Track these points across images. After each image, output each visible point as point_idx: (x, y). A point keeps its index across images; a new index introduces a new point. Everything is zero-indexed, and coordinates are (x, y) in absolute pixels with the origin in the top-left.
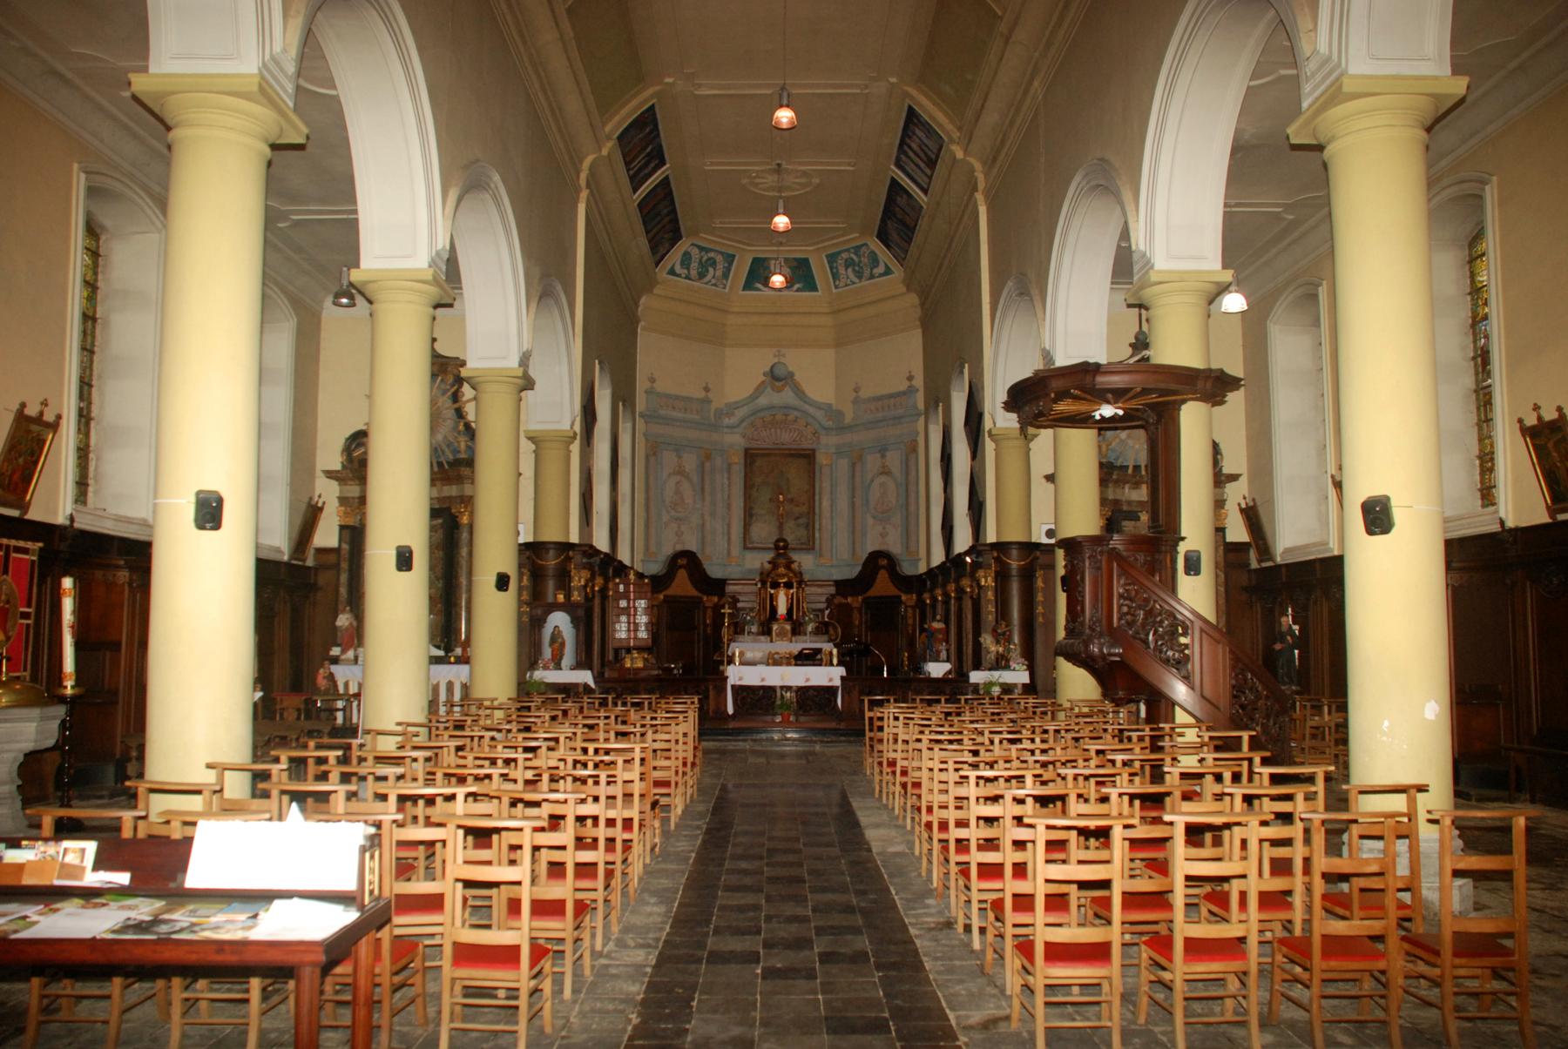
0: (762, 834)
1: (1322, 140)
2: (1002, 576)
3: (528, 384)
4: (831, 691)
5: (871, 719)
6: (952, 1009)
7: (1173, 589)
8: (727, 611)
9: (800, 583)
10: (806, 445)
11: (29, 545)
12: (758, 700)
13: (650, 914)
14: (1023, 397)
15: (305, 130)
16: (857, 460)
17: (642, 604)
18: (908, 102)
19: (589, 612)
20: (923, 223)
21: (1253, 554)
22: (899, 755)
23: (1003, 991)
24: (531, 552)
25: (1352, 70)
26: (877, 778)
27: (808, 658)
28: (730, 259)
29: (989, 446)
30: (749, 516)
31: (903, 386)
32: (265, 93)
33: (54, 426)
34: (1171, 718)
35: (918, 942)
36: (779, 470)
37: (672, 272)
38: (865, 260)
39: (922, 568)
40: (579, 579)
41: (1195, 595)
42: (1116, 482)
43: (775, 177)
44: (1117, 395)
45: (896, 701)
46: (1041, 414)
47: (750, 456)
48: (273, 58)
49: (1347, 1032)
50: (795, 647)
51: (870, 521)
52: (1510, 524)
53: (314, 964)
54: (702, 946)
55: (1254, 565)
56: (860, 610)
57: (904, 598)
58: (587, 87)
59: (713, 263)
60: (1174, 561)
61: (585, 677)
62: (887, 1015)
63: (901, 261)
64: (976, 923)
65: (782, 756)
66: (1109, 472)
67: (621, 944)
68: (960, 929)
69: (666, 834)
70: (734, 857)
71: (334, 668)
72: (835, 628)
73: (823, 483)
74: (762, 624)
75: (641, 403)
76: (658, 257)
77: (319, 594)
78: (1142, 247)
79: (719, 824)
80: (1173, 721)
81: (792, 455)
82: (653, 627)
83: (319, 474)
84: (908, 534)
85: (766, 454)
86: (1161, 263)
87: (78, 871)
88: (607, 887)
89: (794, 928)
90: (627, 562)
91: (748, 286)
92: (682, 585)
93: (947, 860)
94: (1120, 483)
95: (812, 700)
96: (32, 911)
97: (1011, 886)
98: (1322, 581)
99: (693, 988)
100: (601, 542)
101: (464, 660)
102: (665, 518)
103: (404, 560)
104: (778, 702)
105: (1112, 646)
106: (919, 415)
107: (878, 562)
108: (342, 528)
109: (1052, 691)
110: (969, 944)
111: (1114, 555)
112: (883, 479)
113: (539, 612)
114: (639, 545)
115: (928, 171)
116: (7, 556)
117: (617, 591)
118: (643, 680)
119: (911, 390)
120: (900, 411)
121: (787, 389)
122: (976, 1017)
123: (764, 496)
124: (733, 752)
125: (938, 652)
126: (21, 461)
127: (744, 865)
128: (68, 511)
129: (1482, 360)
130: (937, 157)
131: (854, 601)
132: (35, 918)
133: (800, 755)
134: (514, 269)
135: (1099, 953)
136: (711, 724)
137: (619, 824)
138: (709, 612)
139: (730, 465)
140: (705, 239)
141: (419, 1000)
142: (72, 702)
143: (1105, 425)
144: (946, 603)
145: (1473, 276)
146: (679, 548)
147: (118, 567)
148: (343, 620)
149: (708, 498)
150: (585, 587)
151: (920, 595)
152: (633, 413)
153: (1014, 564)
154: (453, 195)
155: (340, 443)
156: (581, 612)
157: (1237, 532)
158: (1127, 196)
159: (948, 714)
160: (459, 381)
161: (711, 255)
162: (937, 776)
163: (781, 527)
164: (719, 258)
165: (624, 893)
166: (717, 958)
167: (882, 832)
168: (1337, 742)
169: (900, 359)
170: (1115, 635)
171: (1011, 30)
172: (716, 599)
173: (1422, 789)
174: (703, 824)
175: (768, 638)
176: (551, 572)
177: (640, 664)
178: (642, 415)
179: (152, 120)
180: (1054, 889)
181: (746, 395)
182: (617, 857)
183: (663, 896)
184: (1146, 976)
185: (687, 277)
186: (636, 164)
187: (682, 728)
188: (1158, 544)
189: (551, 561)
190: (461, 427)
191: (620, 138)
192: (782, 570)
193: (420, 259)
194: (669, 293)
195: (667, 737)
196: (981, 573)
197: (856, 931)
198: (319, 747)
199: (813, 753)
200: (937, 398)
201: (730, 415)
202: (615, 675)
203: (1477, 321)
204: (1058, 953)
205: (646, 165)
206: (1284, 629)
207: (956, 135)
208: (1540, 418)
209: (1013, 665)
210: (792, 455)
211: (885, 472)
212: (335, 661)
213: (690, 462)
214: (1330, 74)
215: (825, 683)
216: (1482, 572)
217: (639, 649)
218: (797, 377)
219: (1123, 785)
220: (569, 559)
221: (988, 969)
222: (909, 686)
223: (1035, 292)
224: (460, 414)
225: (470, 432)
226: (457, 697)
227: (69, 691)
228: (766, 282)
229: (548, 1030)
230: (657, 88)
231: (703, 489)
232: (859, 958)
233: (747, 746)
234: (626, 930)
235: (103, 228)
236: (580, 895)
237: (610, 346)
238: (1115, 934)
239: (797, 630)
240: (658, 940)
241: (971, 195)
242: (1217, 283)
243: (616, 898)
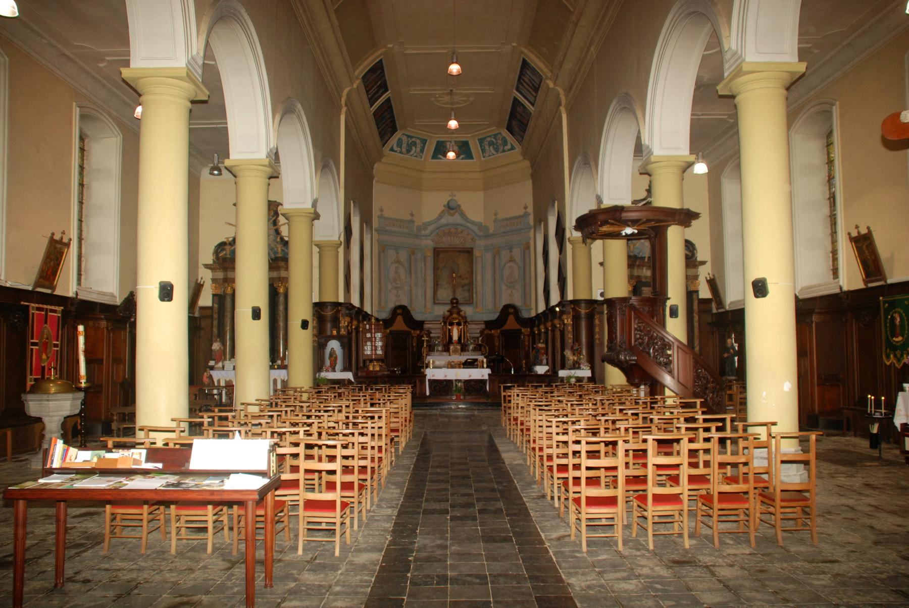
0: (447, 456)
1: (734, 94)
2: (576, 318)
3: (316, 216)
4: (483, 382)
5: (505, 396)
7: (663, 324)
8: (425, 338)
9: (465, 322)
10: (468, 246)
11: (57, 308)
12: (443, 387)
14: (583, 223)
15: (208, 93)
16: (496, 253)
17: (379, 335)
18: (523, 56)
19: (350, 340)
20: (532, 123)
21: (714, 305)
22: (519, 415)
23: (568, 524)
24: (319, 307)
25: (748, 59)
26: (508, 427)
27: (470, 364)
28: (424, 142)
29: (569, 247)
30: (436, 285)
31: (522, 212)
32: (190, 77)
33: (68, 245)
34: (662, 393)
35: (527, 504)
36: (453, 260)
37: (392, 150)
39: (533, 314)
40: (344, 323)
41: (675, 329)
42: (639, 266)
43: (449, 97)
44: (633, 223)
45: (518, 386)
46: (593, 233)
47: (437, 252)
48: (192, 57)
49: (732, 539)
50: (463, 358)
51: (504, 288)
52: (845, 289)
53: (253, 500)
54: (420, 507)
55: (714, 311)
56: (499, 337)
57: (523, 330)
58: (345, 52)
59: (415, 144)
60: (664, 311)
61: (349, 376)
63: (520, 142)
64: (556, 495)
65: (457, 417)
66: (633, 261)
67: (379, 506)
68: (549, 498)
69: (397, 456)
70: (433, 467)
71: (212, 372)
73: (478, 268)
77: (202, 332)
78: (647, 143)
79: (423, 453)
80: (664, 394)
82: (385, 348)
83: (200, 265)
84: (525, 294)
85: (446, 251)
86: (657, 151)
87: (136, 462)
88: (372, 478)
89: (465, 498)
90: (369, 312)
91: (435, 157)
92: (400, 325)
93: (542, 465)
94: (640, 266)
95: (472, 386)
96: (123, 480)
97: (572, 474)
98: (735, 321)
99: (417, 524)
100: (356, 302)
101: (284, 367)
102: (390, 287)
103: (256, 314)
105: (631, 355)
107: (509, 310)
108: (214, 295)
109: (603, 381)
110: (553, 505)
111: (632, 307)
112: (511, 264)
113: (323, 340)
114: (375, 302)
116: (46, 314)
117: (364, 328)
118: (380, 377)
119: (526, 215)
122: (555, 535)
124: (431, 415)
125: (542, 361)
126: (52, 263)
127: (439, 470)
128: (75, 290)
129: (832, 199)
132: (125, 482)
133: (466, 417)
134: (309, 155)
135: (611, 501)
136: (418, 401)
137: (376, 448)
138: (415, 339)
139: (425, 258)
140: (410, 131)
141: (286, 529)
142: (86, 390)
143: (629, 238)
144: (546, 332)
145: (828, 153)
146: (398, 304)
147: (101, 319)
148: (216, 346)
149: (413, 277)
150: (347, 326)
152: (371, 229)
153: (583, 311)
154: (204, 28)
155: (211, 249)
156: (346, 340)
157: (705, 293)
158: (639, 115)
159: (546, 393)
161: (414, 140)
162: (545, 430)
163: (454, 292)
164: (418, 142)
165: (379, 484)
166: (426, 512)
167: (511, 454)
168: (741, 404)
169: (520, 197)
170: (632, 350)
171: (578, 20)
172: (418, 332)
173: (774, 424)
174: (416, 451)
175: (454, 354)
176: (329, 319)
177: (378, 369)
178: (376, 230)
179: (131, 90)
180: (591, 474)
182: (376, 465)
183: (398, 485)
184: (636, 514)
185: (401, 152)
186: (372, 91)
187: (403, 402)
189: (329, 313)
190: (278, 240)
191: (363, 78)
192: (455, 316)
193: (262, 154)
194: (390, 161)
195: (396, 406)
196: (564, 317)
197: (496, 500)
198: (220, 411)
199: (474, 416)
200: (541, 219)
201: (425, 229)
202: (364, 374)
203: (830, 179)
204: (593, 501)
205: (377, 92)
206: (729, 345)
207: (549, 74)
208: (859, 233)
209: (582, 366)
211: (512, 260)
212: (212, 368)
213: (403, 256)
214: (737, 60)
215: (480, 378)
216: (817, 317)
217: (377, 360)
220: (338, 311)
221: (562, 515)
222: (526, 378)
223: (592, 163)
224: (277, 232)
225: (286, 244)
226: (279, 387)
227: (83, 385)
228: (445, 155)
229: (348, 542)
230: (383, 50)
232: (498, 511)
233: (437, 412)
234: (380, 500)
235: (86, 135)
236: (345, 500)
237: (359, 193)
238: (620, 492)
239: (464, 349)
241: (558, 109)
242: (792, 73)
243: (375, 484)
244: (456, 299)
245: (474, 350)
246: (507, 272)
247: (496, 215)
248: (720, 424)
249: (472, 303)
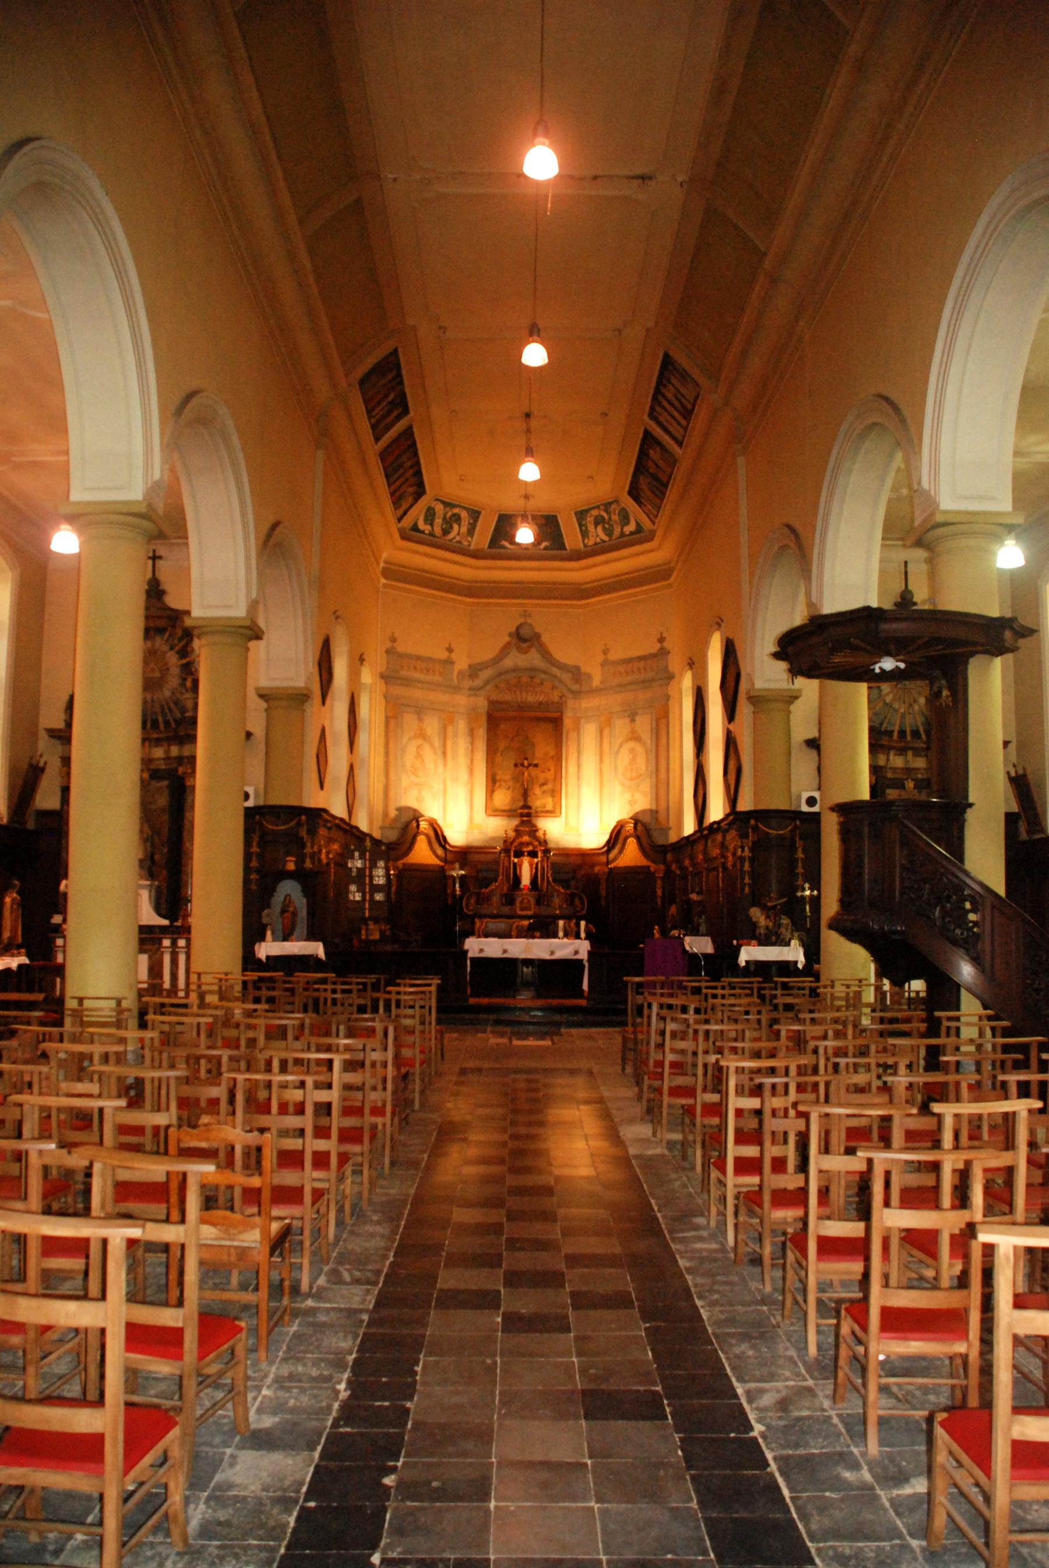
4: (572, 966)
6: (740, 1379)
13: (373, 1235)
28: (475, 515)
38: (615, 517)
59: (457, 519)
61: (318, 949)
62: (659, 1388)
76: (400, 511)
94: (886, 749)
95: (556, 975)
115: (684, 422)
121: (533, 650)
130: (694, 406)
134: (243, 515)
160: (188, 635)
161: (456, 510)
164: (464, 515)
177: (376, 936)
181: (491, 656)
186: (378, 412)
188: (950, 814)
205: (389, 412)
218: (545, 638)
219: (901, 1080)
240: (378, 1273)
247: (605, 652)
248: (1020, 1056)
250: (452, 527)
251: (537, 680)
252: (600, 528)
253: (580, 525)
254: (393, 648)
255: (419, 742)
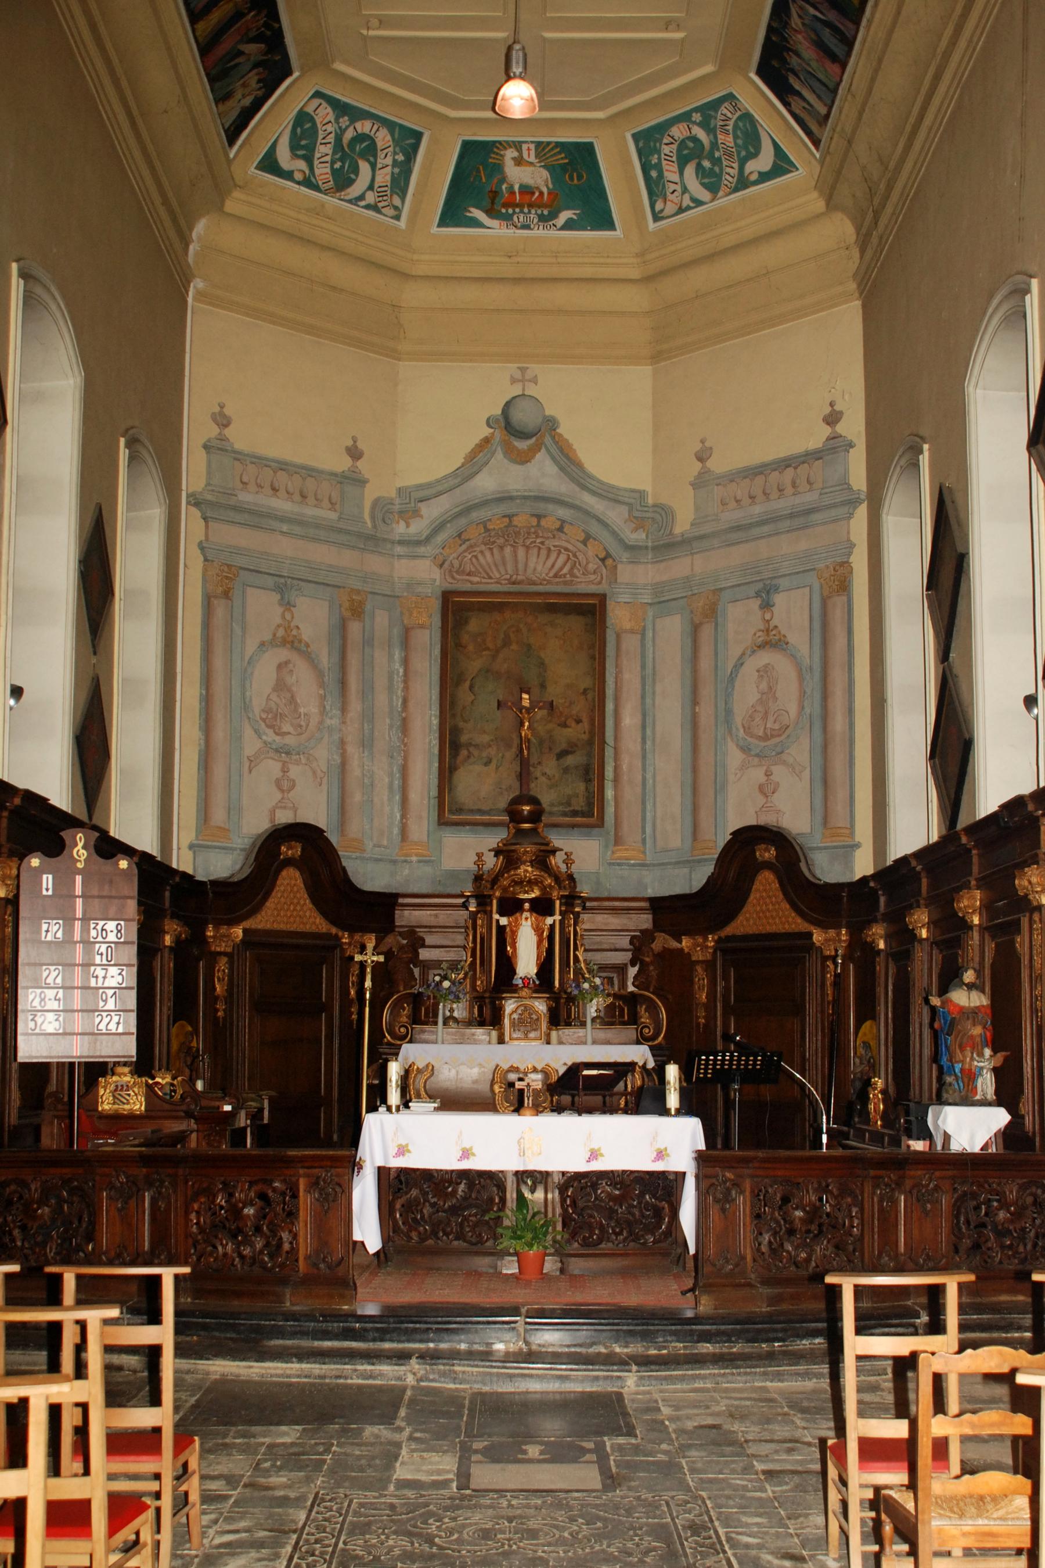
4: (663, 1186)
9: (571, 900)
10: (585, 585)
28: (409, 141)
30: (452, 748)
31: (817, 437)
36: (520, 654)
37: (270, 164)
38: (727, 140)
39: (863, 866)
47: (456, 610)
50: (561, 1054)
51: (734, 757)
57: (818, 937)
59: (368, 148)
72: (652, 1009)
73: (625, 675)
74: (478, 999)
75: (194, 471)
81: (552, 609)
84: (825, 784)
85: (492, 605)
91: (452, 214)
95: (615, 1211)
102: (251, 745)
104: (509, 1219)
106: (853, 503)
112: (765, 658)
119: (836, 446)
120: (809, 498)
121: (541, 456)
123: (482, 704)
125: (971, 1076)
131: (697, 947)
139: (407, 633)
146: (284, 818)
149: (355, 706)
151: (857, 930)
161: (365, 127)
163: (524, 775)
164: (383, 138)
178: (196, 502)
185: (308, 183)
192: (526, 870)
201: (409, 514)
210: (552, 609)
211: (772, 640)
213: (313, 617)
215: (643, 1162)
231: (343, 683)
233: (409, 1375)
239: (562, 1015)
244: (534, 801)
245: (610, 1018)
246: (747, 693)
249: (601, 823)
250: (356, 170)
251: (547, 523)
252: (690, 170)
253: (645, 169)
254: (222, 438)
255: (284, 654)
